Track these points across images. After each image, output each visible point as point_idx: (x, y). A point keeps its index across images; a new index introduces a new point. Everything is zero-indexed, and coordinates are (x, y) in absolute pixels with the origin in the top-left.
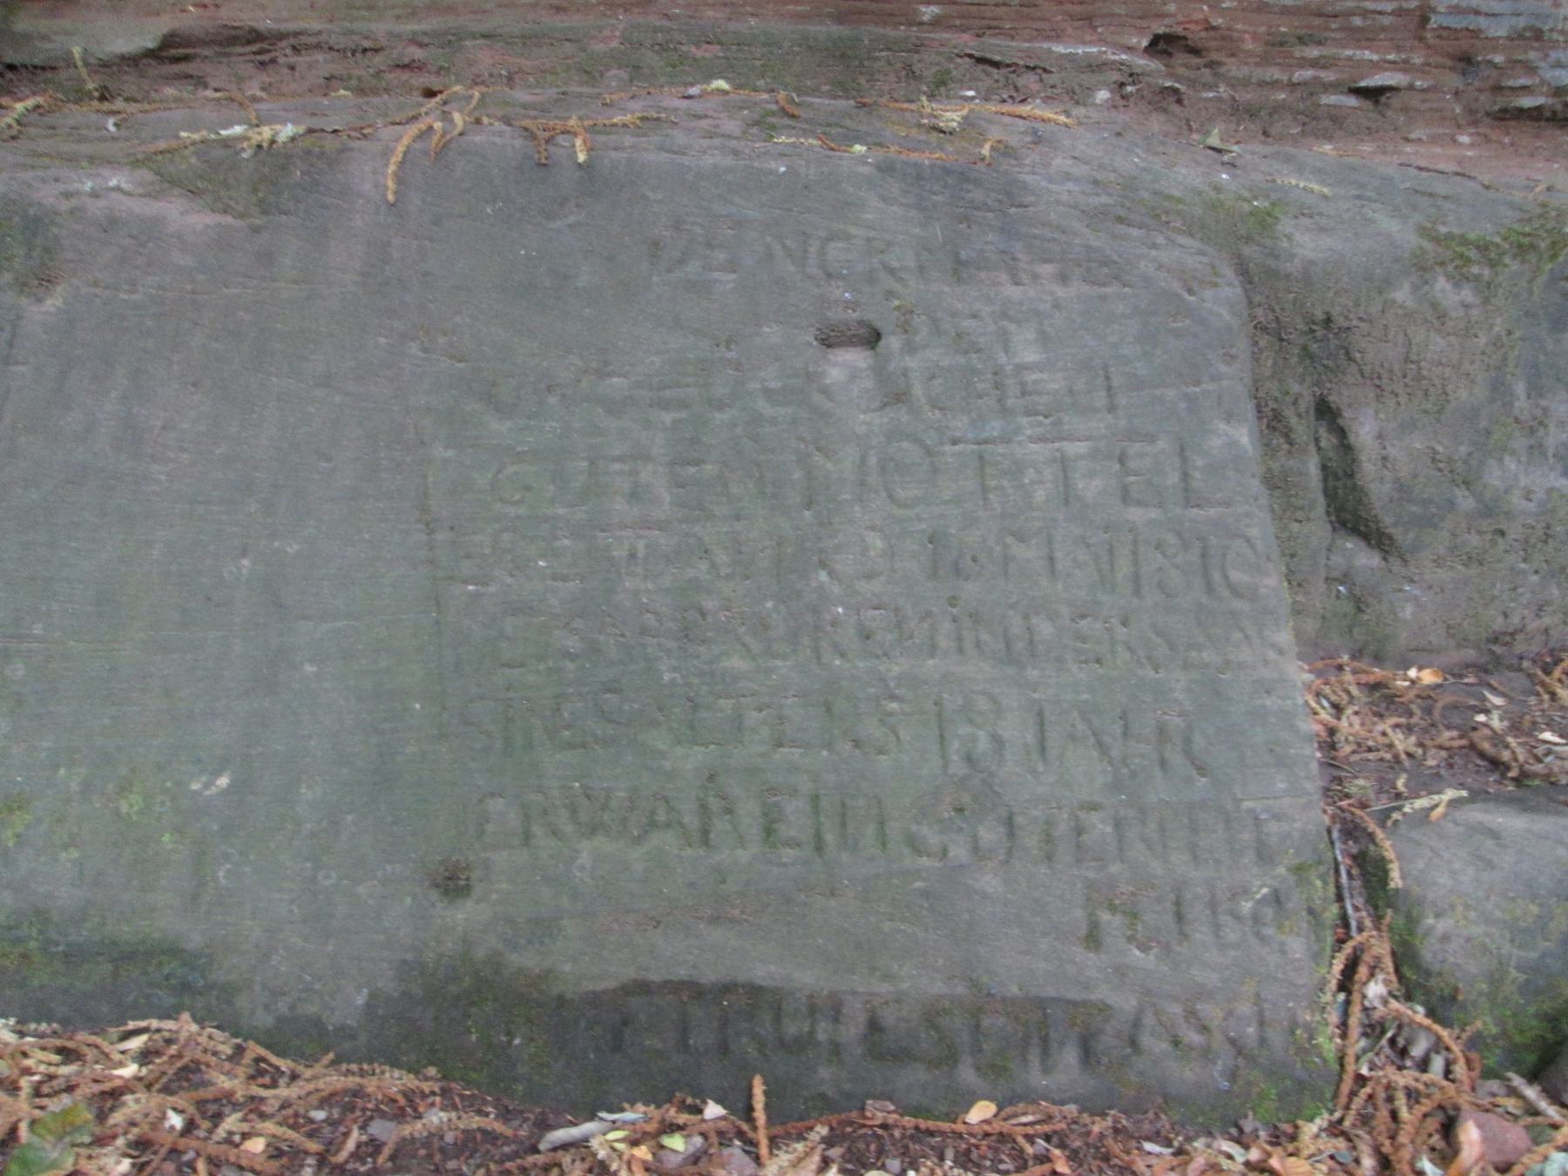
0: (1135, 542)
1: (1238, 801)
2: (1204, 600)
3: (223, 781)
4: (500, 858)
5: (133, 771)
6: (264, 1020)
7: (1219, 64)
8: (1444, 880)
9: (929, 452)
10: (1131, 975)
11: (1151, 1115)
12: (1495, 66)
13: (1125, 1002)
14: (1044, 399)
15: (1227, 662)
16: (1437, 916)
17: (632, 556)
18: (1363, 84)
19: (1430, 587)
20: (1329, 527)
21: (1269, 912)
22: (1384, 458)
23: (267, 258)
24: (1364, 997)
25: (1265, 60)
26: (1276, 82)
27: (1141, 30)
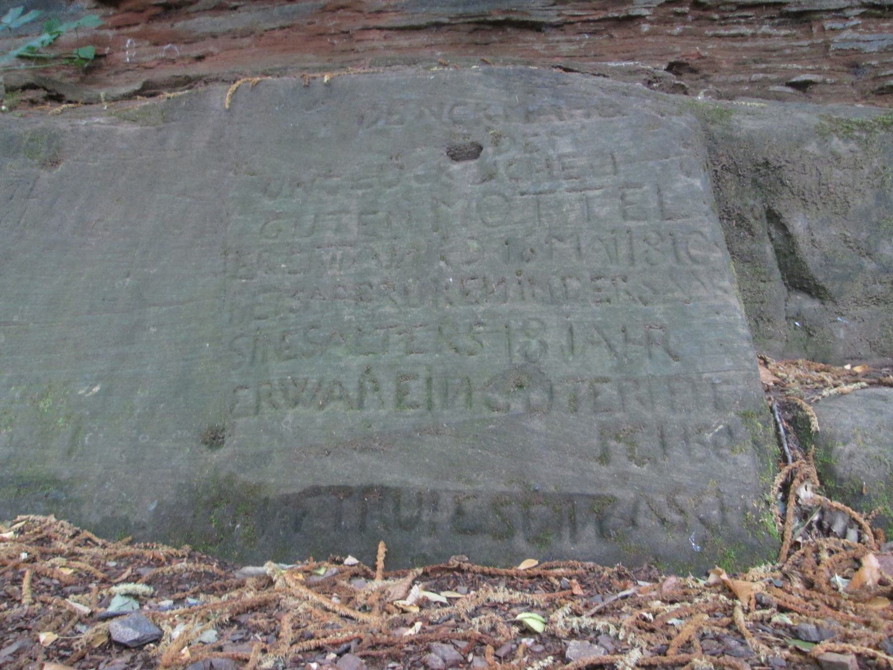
0: (631, 239)
1: (700, 374)
2: (675, 265)
3: (96, 389)
4: (241, 421)
5: (50, 387)
6: (96, 519)
7: (709, 76)
8: (848, 422)
9: (507, 200)
10: (630, 479)
11: (645, 567)
12: (873, 67)
13: (626, 495)
14: (576, 170)
15: (691, 298)
16: (845, 444)
17: (334, 259)
18: (794, 80)
19: (855, 319)
20: (785, 289)
21: (724, 440)
22: (813, 241)
23: (163, 141)
24: (798, 497)
25: (736, 72)
26: (742, 81)
27: (661, 61)
